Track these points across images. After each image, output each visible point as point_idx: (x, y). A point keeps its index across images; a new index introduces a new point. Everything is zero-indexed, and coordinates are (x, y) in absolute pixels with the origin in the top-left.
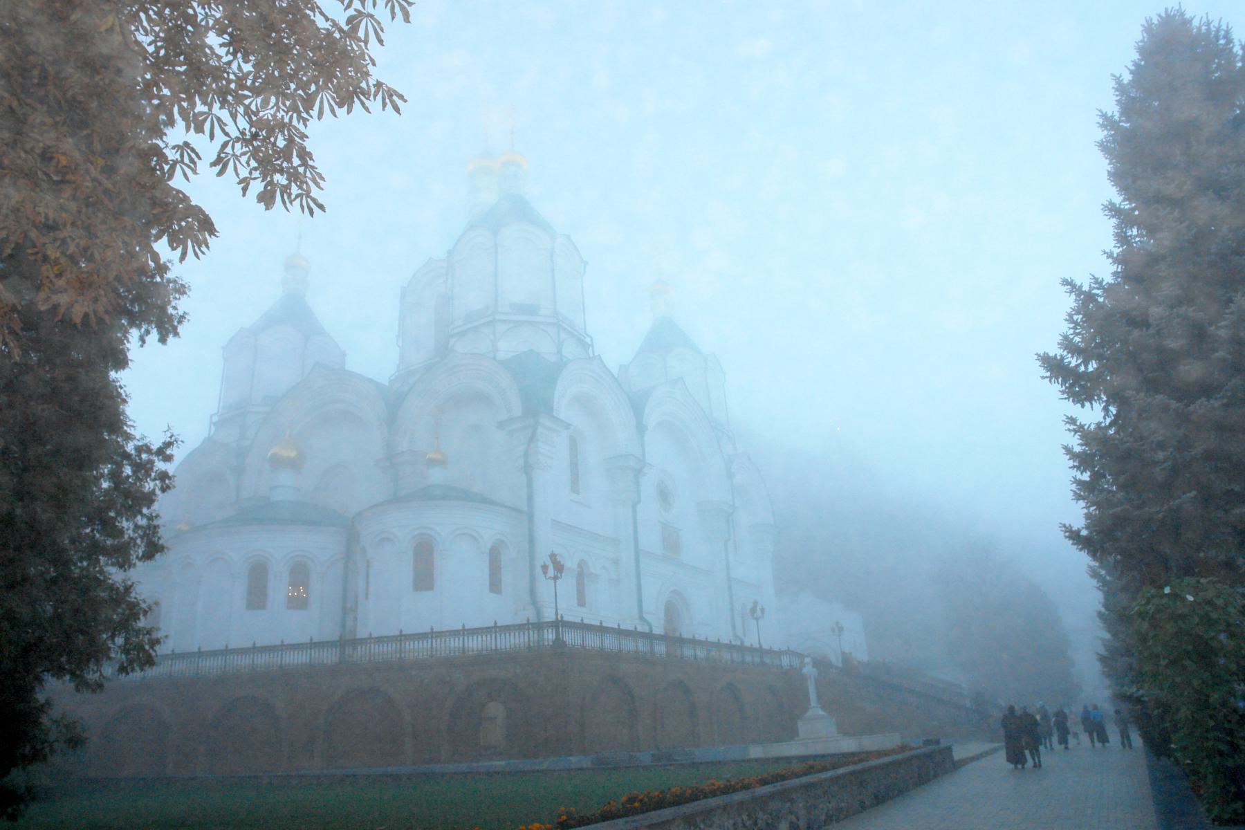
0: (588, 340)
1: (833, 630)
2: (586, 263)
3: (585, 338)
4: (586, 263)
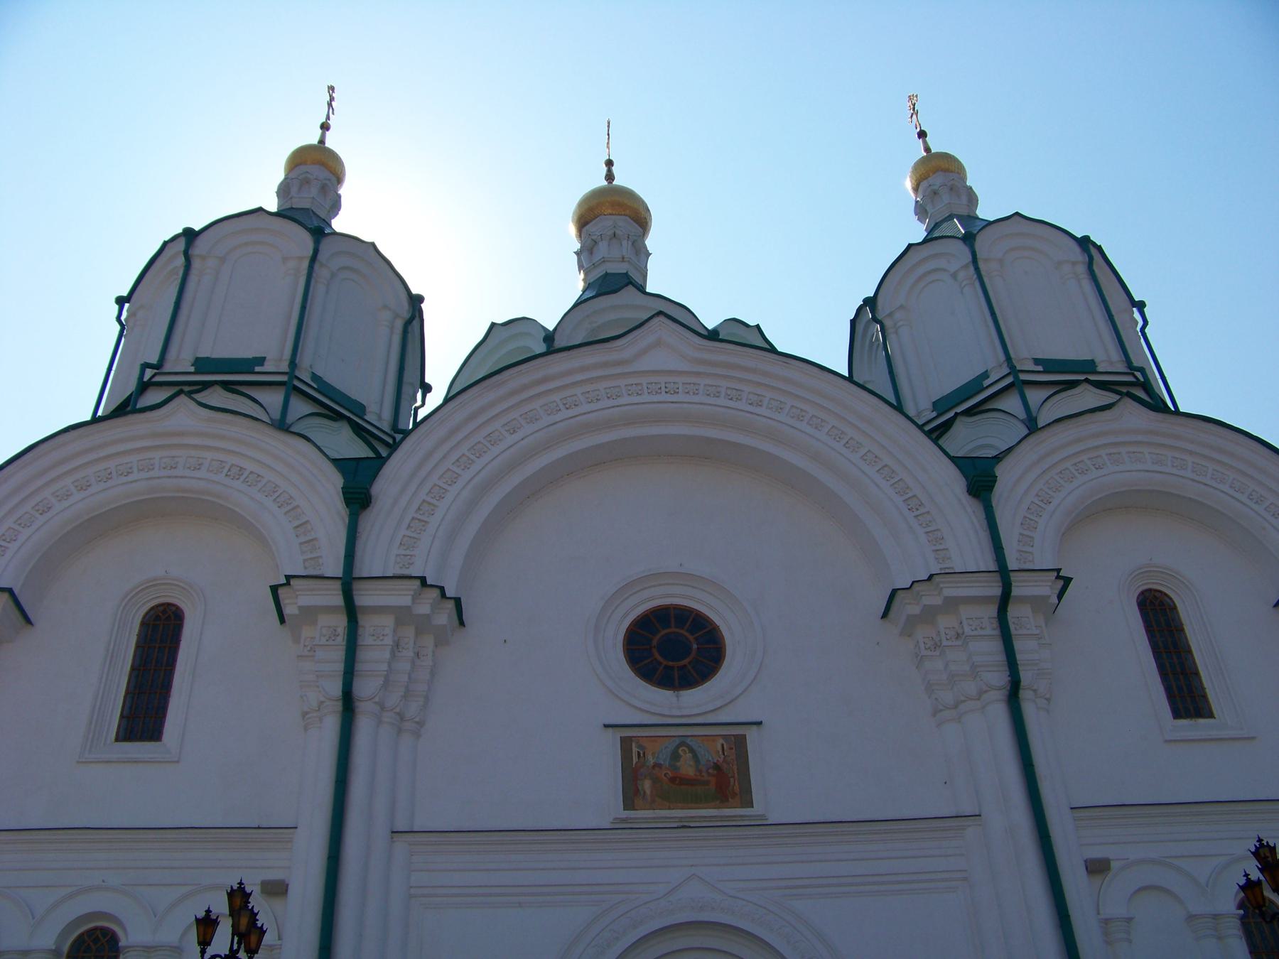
1: (207, 925)
2: (1141, 306)
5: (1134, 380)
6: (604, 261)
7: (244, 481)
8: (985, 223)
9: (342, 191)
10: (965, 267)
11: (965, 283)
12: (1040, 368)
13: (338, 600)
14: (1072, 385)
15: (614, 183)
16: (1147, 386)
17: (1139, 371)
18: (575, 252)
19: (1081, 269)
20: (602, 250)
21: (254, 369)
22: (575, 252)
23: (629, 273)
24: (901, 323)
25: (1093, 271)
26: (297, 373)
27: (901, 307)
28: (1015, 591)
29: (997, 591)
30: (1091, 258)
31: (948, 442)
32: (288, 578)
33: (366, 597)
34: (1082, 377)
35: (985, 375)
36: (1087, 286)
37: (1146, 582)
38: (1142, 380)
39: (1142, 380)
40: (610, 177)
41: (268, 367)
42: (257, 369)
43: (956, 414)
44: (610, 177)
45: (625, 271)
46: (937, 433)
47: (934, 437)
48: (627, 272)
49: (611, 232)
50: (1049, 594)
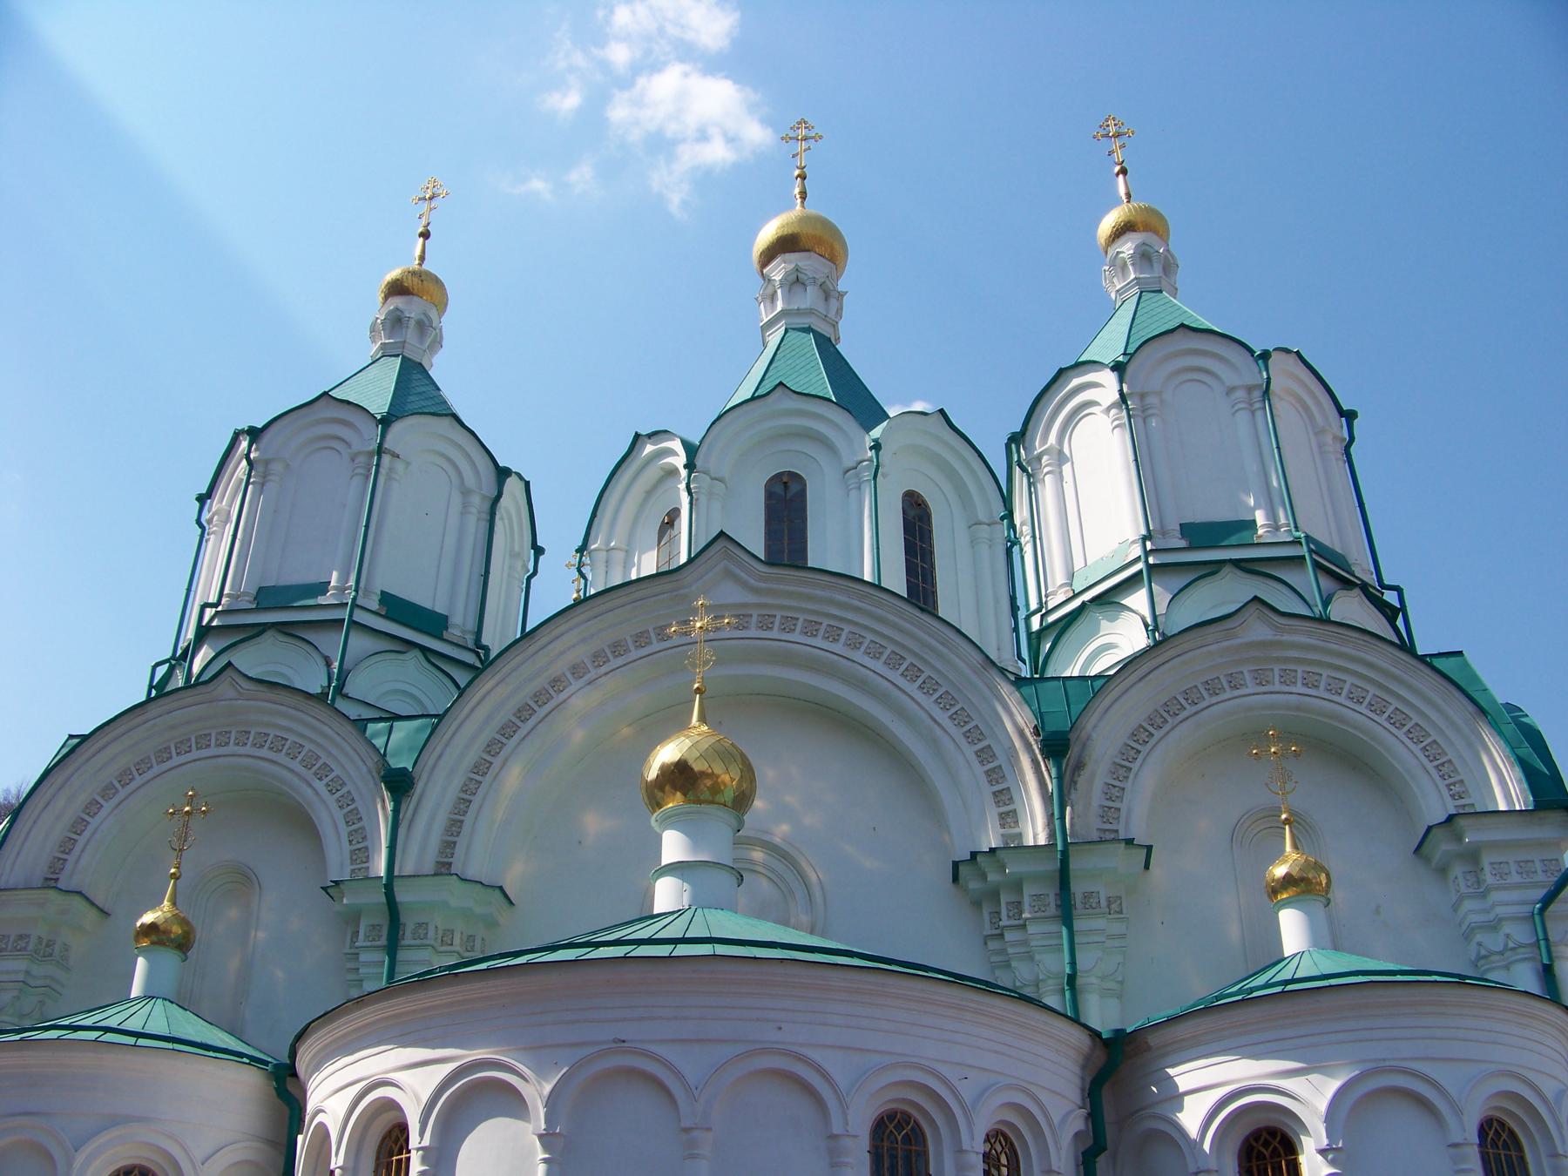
0: (1391, 597)
2: (1349, 416)
3: (1383, 594)
4: (1349, 416)
14: (1214, 567)
32: (337, 883)
45: (807, 326)
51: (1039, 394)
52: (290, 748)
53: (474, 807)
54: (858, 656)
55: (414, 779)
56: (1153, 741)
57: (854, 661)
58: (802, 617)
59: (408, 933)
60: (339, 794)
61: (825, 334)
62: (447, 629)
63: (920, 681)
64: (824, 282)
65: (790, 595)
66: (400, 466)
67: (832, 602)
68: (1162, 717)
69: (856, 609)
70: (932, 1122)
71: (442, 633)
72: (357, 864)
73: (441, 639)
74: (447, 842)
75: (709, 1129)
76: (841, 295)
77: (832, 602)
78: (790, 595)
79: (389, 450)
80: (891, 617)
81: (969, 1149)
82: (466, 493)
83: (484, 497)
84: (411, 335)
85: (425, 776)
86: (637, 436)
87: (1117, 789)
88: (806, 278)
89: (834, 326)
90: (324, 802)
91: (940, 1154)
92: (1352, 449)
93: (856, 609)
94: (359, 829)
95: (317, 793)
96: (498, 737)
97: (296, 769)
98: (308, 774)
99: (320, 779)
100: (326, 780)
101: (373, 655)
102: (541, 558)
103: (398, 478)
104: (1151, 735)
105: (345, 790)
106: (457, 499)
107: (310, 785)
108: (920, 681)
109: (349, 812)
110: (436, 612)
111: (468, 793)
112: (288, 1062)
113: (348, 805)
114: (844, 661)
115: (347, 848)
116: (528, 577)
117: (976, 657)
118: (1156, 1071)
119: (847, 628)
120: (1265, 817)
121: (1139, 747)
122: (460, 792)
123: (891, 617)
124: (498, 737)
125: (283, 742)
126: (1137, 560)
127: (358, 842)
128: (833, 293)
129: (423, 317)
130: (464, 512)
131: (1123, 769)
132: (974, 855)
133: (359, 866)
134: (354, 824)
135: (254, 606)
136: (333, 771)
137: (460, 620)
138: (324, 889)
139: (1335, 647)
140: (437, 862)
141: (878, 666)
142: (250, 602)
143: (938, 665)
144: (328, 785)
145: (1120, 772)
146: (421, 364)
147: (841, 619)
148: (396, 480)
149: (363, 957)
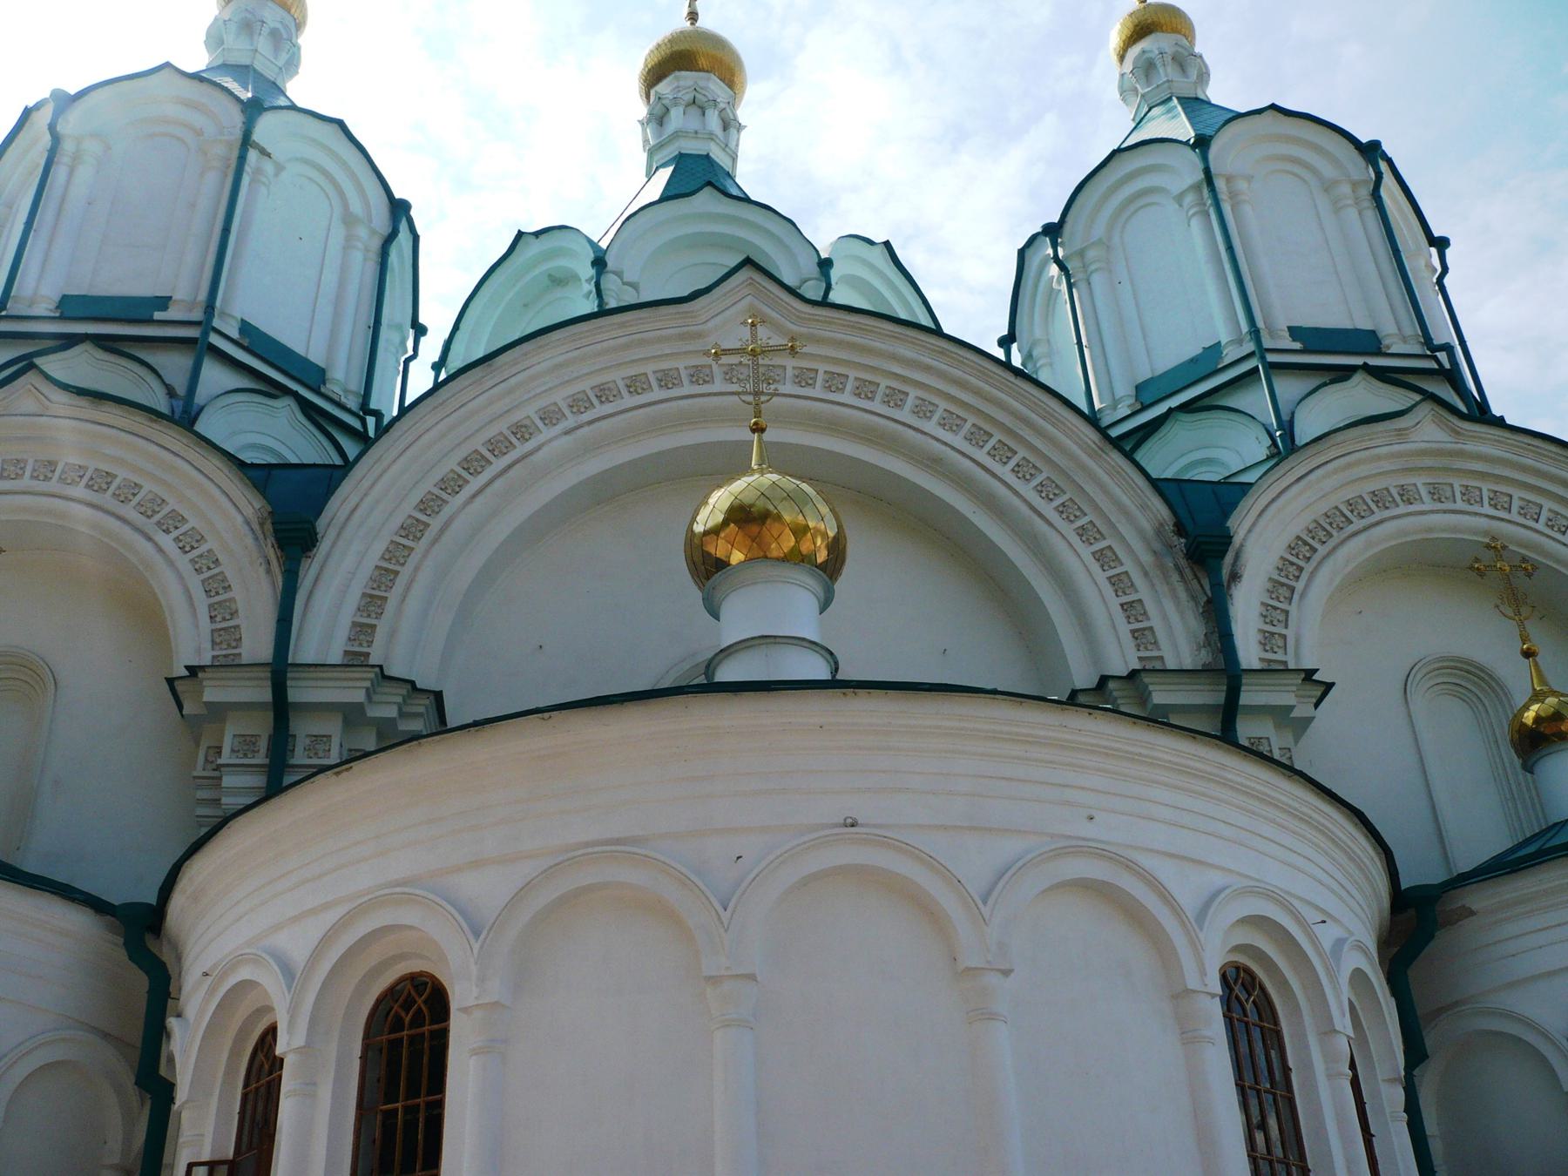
2: (1441, 244)
5: (1436, 366)
6: (676, 135)
7: (193, 561)
8: (1230, 115)
9: (301, 41)
10: (1196, 187)
11: (1191, 213)
12: (1297, 346)
13: (266, 695)
14: (1344, 373)
15: (697, 25)
16: (1452, 377)
17: (1443, 350)
18: (639, 121)
19: (1365, 192)
20: (676, 119)
21: (152, 316)
22: (639, 121)
23: (711, 154)
24: (1093, 267)
25: (1380, 197)
26: (216, 323)
27: (1100, 242)
28: (1245, 698)
29: (1219, 698)
30: (1379, 176)
31: (1148, 456)
32: (193, 671)
33: (298, 693)
34: (1358, 361)
35: (163, 302)
36: (1371, 216)
37: (1458, 681)
38: (1447, 366)
39: (1447, 366)
40: (693, 16)
41: (172, 314)
42: (158, 315)
43: (1170, 410)
44: (693, 16)
45: (705, 153)
46: (1129, 444)
47: (1128, 448)
48: (708, 154)
49: (688, 97)
50: (1295, 704)
51: (1083, 181)
52: (119, 488)
53: (401, 581)
54: (930, 426)
55: (316, 534)
56: (1317, 557)
57: (925, 434)
58: (852, 374)
59: (299, 750)
60: (196, 553)
61: (725, 167)
62: (325, 384)
63: (1012, 463)
64: (724, 109)
65: (839, 344)
66: (268, 167)
67: (894, 358)
68: (1324, 529)
69: (928, 369)
70: (1283, 984)
71: (320, 387)
72: (221, 649)
73: (150, 321)
74: (362, 625)
75: (1006, 973)
76: (740, 128)
77: (894, 358)
78: (839, 344)
79: (257, 144)
80: (973, 380)
81: (1342, 1030)
82: (349, 220)
83: (373, 232)
84: (263, 44)
85: (331, 534)
86: (520, 234)
87: (1278, 612)
88: (705, 99)
89: (734, 159)
90: (171, 564)
91: (1301, 1037)
92: (1446, 281)
93: (928, 369)
94: (225, 601)
95: (160, 550)
96: (436, 491)
97: (127, 516)
98: (149, 525)
99: (167, 531)
100: (175, 533)
101: (221, 395)
102: (423, 339)
103: (264, 179)
104: (1314, 550)
105: (204, 548)
106: (338, 234)
107: (149, 539)
108: (1012, 463)
109: (209, 578)
110: (309, 360)
111: (393, 562)
112: (155, 904)
113: (209, 568)
114: (911, 432)
115: (206, 625)
116: (406, 359)
117: (1091, 436)
118: (1488, 945)
119: (913, 393)
120: (1434, 670)
121: (1301, 563)
122: (379, 560)
123: (973, 380)
124: (436, 491)
125: (109, 480)
126: (1251, 355)
127: (224, 619)
128: (733, 123)
129: (279, 26)
130: (348, 245)
131: (1283, 588)
132: (1104, 680)
133: (224, 652)
134: (217, 593)
135: (57, 315)
136: (187, 521)
137: (343, 378)
138: (171, 682)
139: (1530, 462)
140: (345, 651)
141: (958, 441)
142: (51, 310)
143: (1038, 443)
144: (177, 540)
145: (1280, 591)
146: (274, 83)
147: (904, 380)
148: (264, 184)
149: (228, 781)
